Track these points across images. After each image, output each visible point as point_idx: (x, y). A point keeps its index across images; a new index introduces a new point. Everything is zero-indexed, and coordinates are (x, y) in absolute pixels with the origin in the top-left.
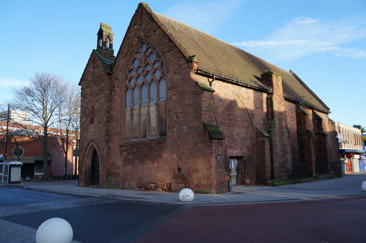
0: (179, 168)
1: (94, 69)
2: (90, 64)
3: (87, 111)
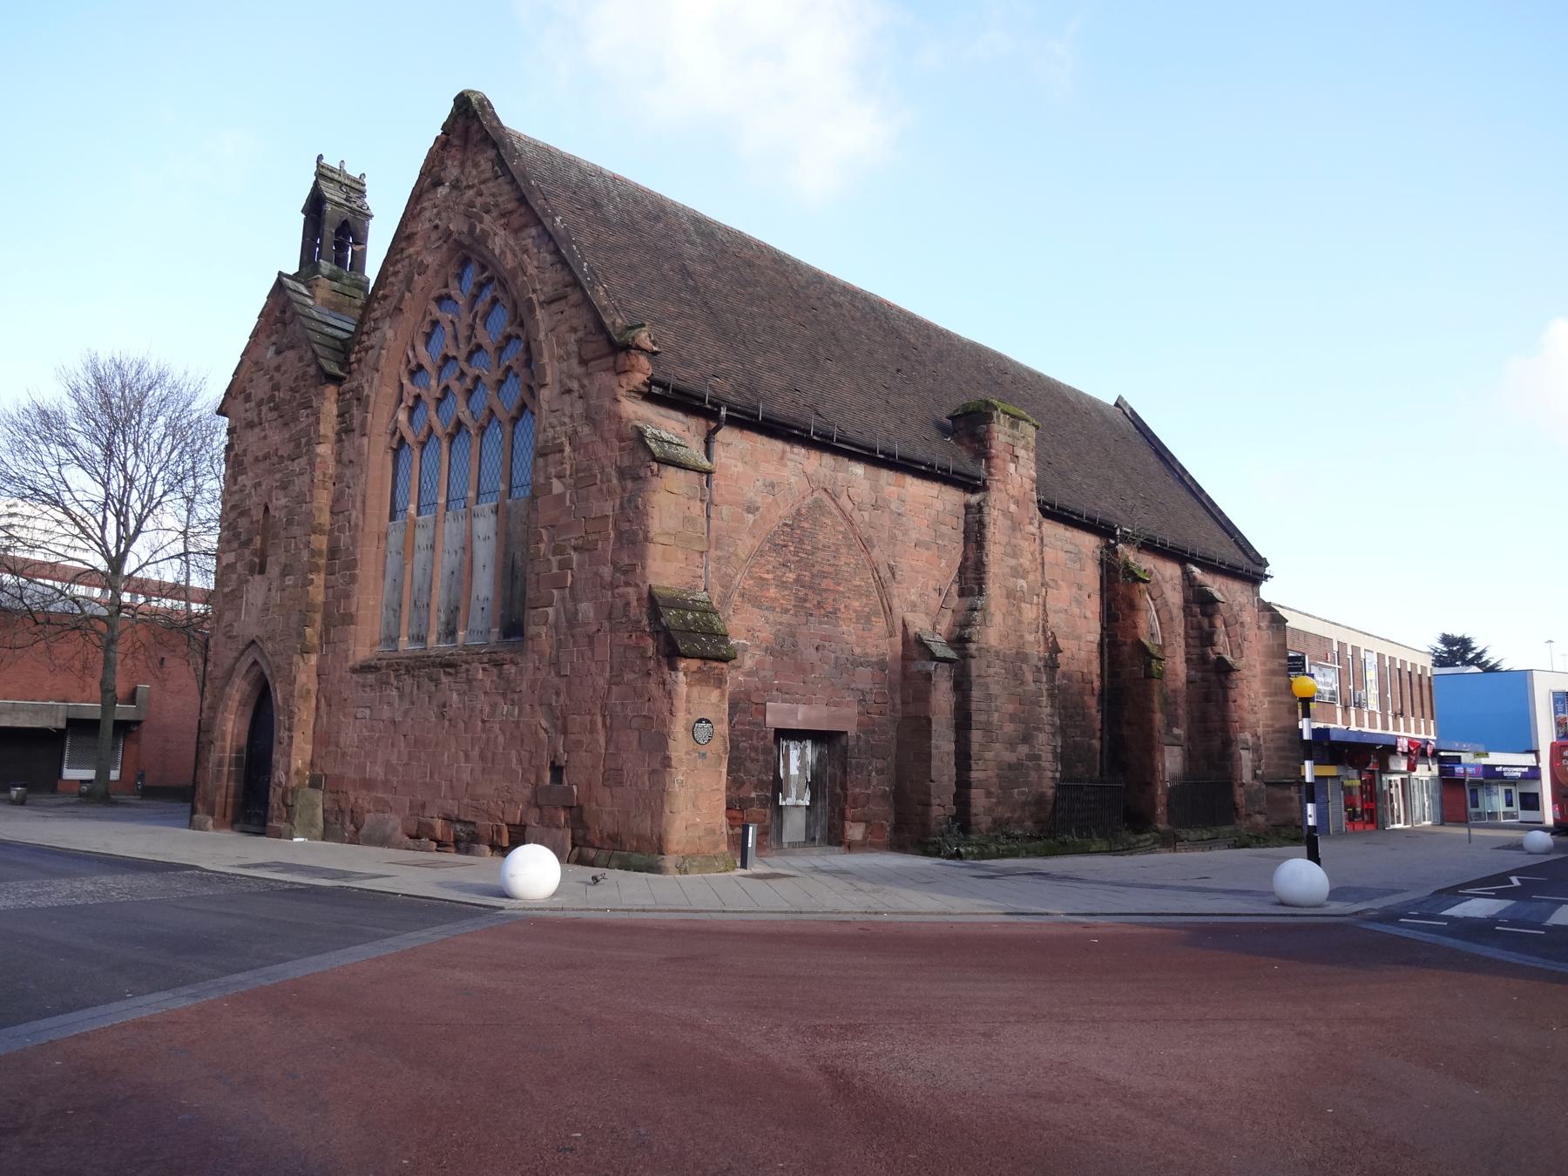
0: (557, 763)
1: (278, 352)
3: (243, 523)
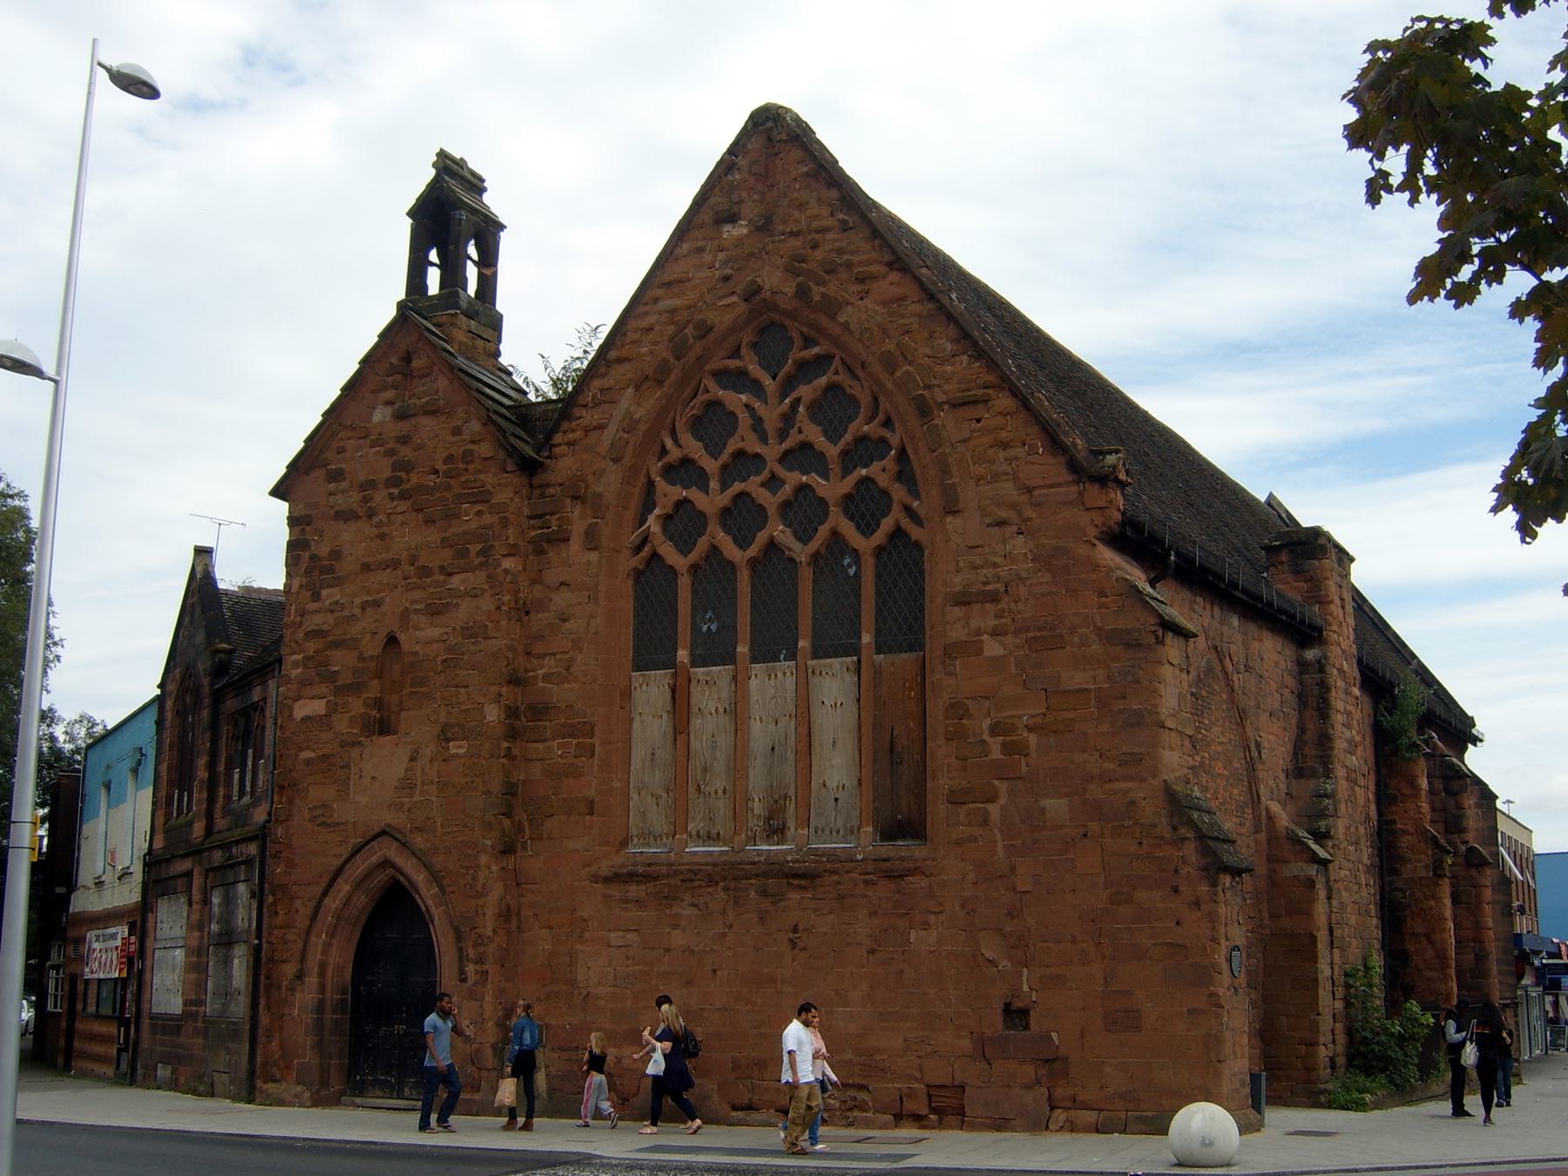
1: (401, 416)
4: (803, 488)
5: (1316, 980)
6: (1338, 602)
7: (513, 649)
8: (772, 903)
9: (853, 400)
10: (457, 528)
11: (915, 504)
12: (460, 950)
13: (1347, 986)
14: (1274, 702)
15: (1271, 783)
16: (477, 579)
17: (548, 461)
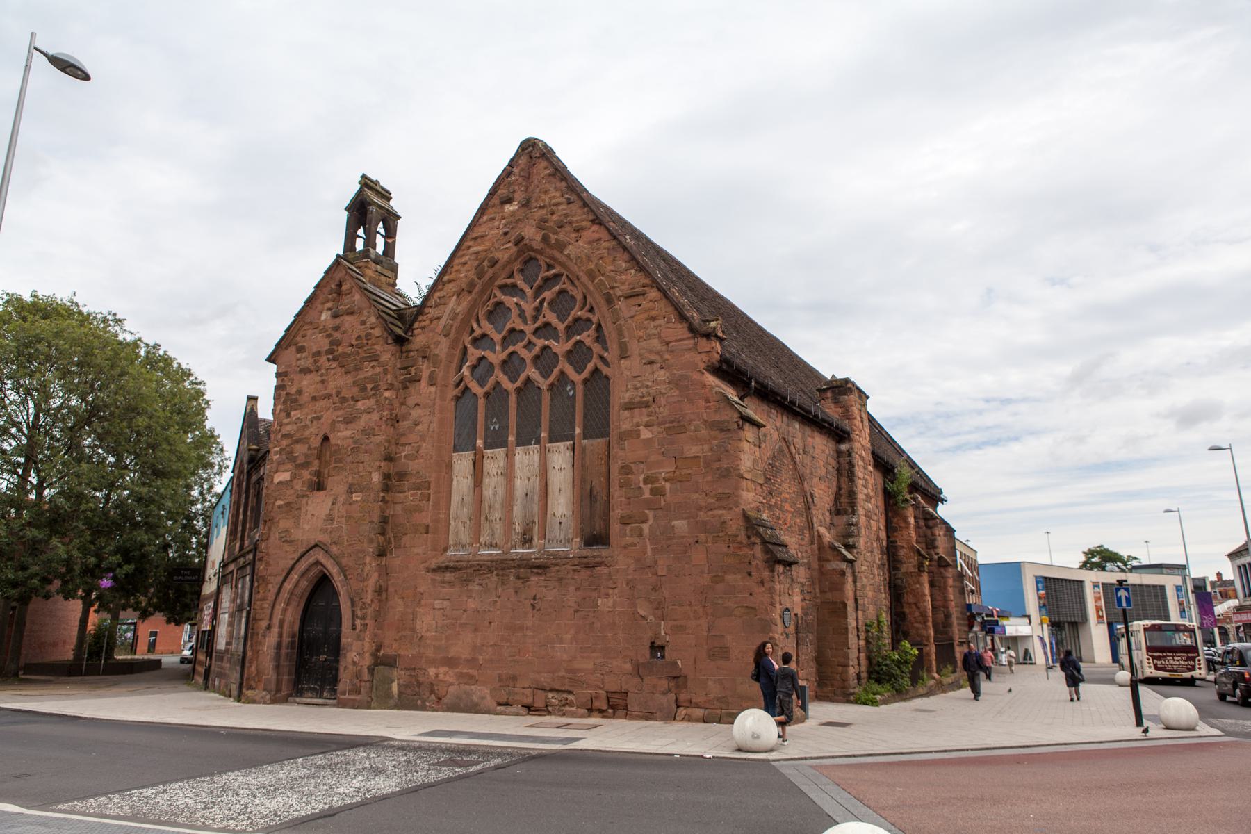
1: (335, 316)
2: (321, 298)
4: (545, 348)
5: (847, 628)
6: (859, 418)
7: (389, 442)
8: (523, 583)
9: (573, 297)
10: (361, 376)
11: (605, 355)
12: (353, 612)
13: (867, 631)
14: (822, 472)
15: (821, 517)
16: (371, 403)
17: (411, 338)
